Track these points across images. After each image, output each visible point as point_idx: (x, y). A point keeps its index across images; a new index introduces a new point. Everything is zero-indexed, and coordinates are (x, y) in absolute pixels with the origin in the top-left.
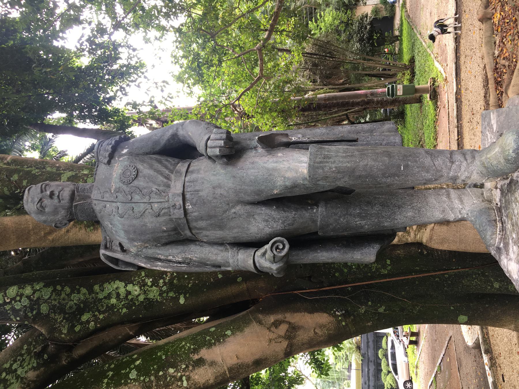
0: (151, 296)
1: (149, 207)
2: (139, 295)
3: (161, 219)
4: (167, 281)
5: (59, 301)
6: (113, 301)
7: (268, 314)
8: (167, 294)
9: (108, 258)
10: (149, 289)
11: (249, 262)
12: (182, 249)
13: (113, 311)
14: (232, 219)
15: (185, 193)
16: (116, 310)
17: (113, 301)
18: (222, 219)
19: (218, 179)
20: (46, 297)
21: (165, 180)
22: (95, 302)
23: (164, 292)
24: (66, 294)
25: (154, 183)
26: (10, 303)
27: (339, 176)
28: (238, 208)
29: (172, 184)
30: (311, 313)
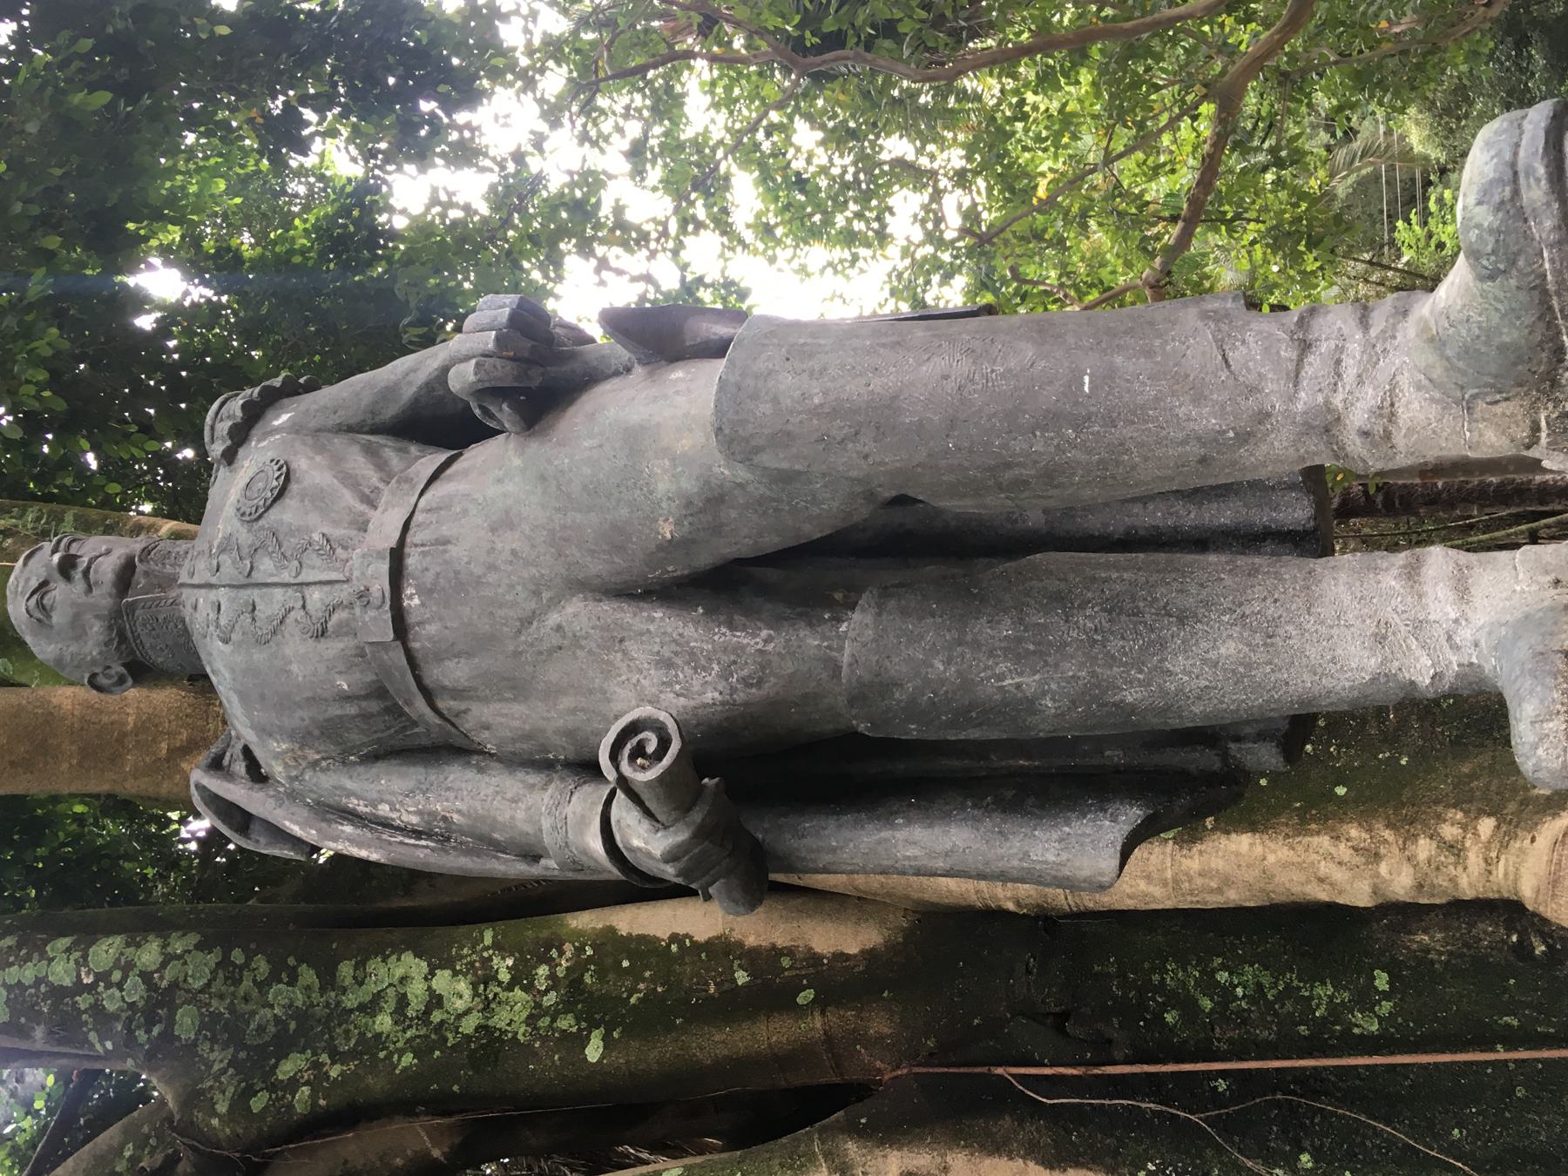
0: (500, 1019)
1: (292, 597)
2: (467, 1012)
3: (333, 647)
5: (232, 1002)
6: (384, 1023)
7: (881, 1143)
8: (554, 1020)
10: (503, 995)
13: (374, 1056)
14: (551, 652)
15: (407, 550)
16: (382, 1055)
18: (517, 654)
20: (198, 985)
21: (362, 507)
22: (329, 1017)
24: (254, 981)
26: (91, 988)
27: (839, 428)
28: (570, 610)
29: (375, 516)
30: (1052, 1168)
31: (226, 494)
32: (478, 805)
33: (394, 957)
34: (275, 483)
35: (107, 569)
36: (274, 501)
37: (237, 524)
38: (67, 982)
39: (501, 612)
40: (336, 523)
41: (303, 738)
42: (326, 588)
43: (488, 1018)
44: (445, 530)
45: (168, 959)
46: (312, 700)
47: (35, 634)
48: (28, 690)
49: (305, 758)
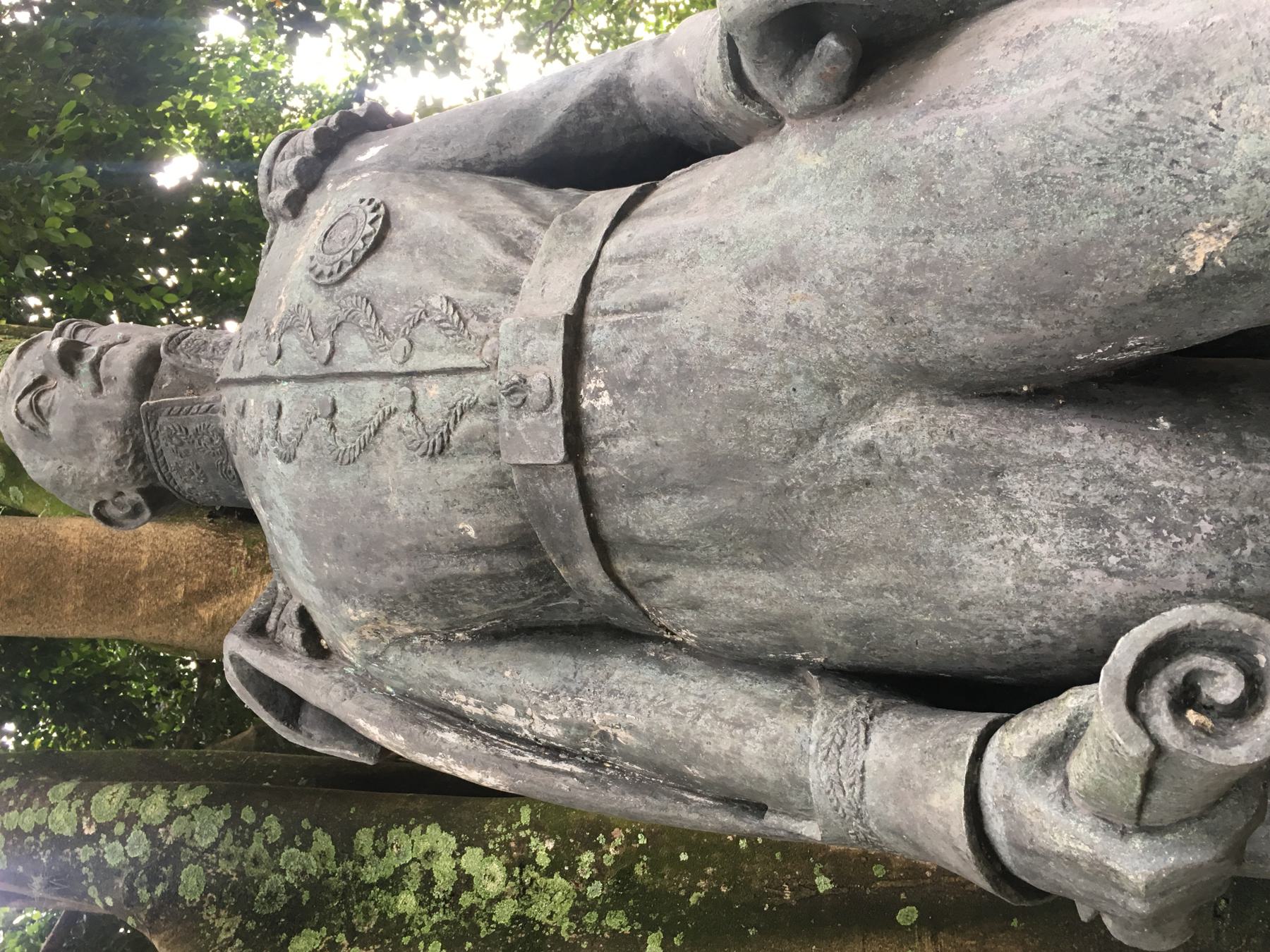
0: (539, 911)
1: (395, 393)
2: (500, 897)
3: (459, 471)
4: (608, 861)
5: (240, 865)
8: (602, 917)
9: (255, 679)
10: (541, 881)
11: (935, 801)
12: (569, 672)
13: (397, 941)
15: (589, 321)
16: (406, 940)
17: (407, 902)
18: (783, 490)
19: (784, 222)
20: (205, 843)
21: (503, 259)
22: (346, 892)
23: (592, 905)
24: (265, 843)
25: (446, 271)
26: (93, 839)
29: (530, 275)
31: (291, 254)
32: (667, 723)
33: (419, 828)
34: (369, 229)
35: (122, 361)
36: (368, 254)
37: (310, 290)
38: (68, 832)
39: (760, 420)
40: (466, 283)
41: (392, 604)
42: (452, 380)
43: (526, 908)
44: (656, 289)
45: (175, 813)
46: (416, 551)
47: (28, 447)
48: (33, 520)
49: (390, 631)
